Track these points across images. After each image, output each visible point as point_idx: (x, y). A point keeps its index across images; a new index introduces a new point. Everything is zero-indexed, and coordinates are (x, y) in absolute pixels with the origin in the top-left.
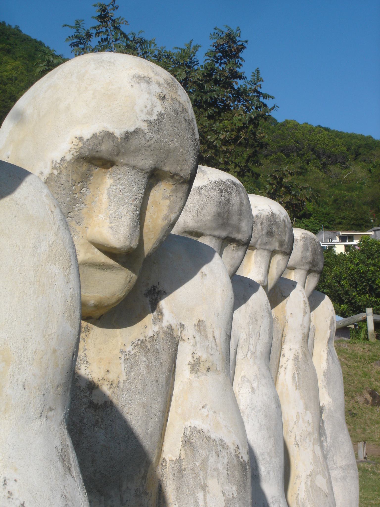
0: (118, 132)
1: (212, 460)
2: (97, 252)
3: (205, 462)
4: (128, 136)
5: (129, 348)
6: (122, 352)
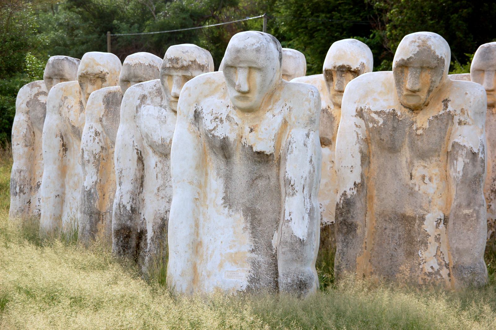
0: (405, 59)
1: (460, 152)
2: (20, 97)
3: (457, 152)
4: (408, 59)
5: (431, 118)
6: (428, 119)
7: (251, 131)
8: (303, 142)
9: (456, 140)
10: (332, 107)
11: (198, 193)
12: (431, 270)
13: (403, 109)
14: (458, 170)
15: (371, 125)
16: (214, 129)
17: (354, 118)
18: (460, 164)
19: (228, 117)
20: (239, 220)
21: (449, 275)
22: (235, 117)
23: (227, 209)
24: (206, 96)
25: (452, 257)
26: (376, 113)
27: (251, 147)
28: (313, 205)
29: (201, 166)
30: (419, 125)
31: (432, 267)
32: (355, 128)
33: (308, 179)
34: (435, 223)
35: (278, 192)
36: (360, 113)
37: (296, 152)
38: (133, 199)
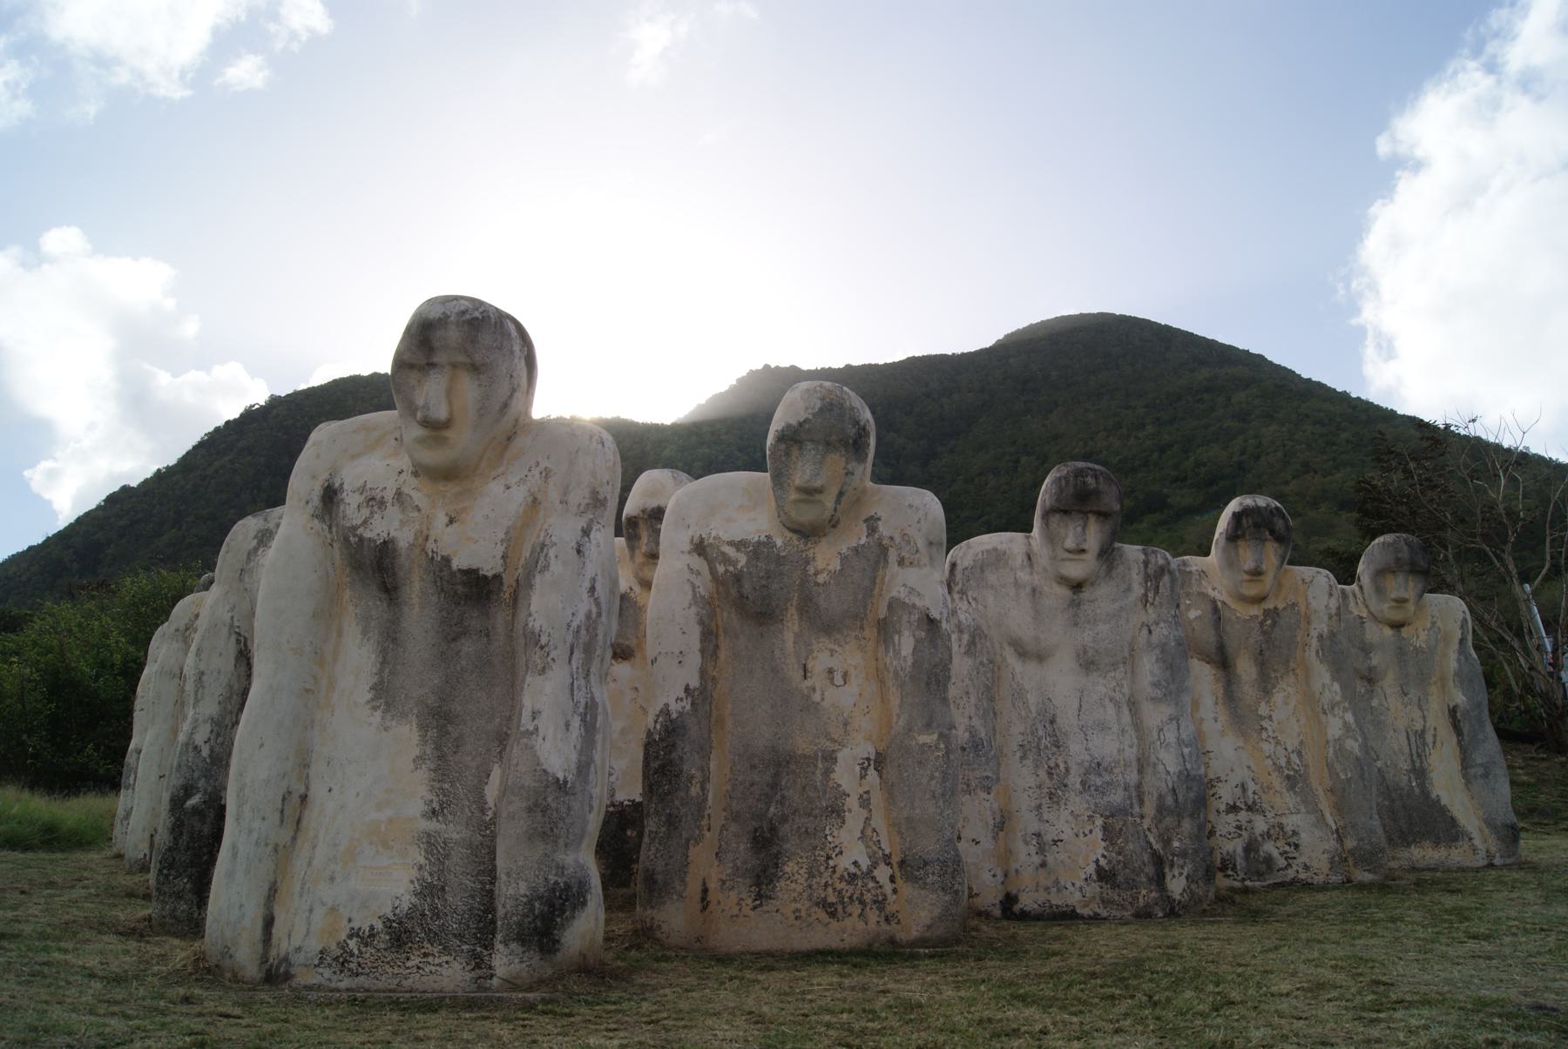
1: (905, 618)
4: (800, 424)
7: (451, 521)
8: (573, 544)
9: (894, 594)
10: (637, 589)
11: (315, 678)
12: (853, 869)
13: (789, 534)
14: (903, 653)
15: (721, 569)
16: (365, 522)
17: (686, 556)
18: (906, 643)
19: (399, 494)
20: (407, 736)
21: (892, 879)
22: (414, 494)
23: (378, 714)
24: (353, 457)
25: (898, 839)
26: (731, 543)
27: (447, 560)
28: (592, 698)
29: (326, 615)
30: (820, 564)
31: (855, 863)
32: (688, 575)
33: (583, 632)
34: (858, 768)
35: (505, 672)
36: (700, 548)
37: (556, 567)
38: (218, 735)
